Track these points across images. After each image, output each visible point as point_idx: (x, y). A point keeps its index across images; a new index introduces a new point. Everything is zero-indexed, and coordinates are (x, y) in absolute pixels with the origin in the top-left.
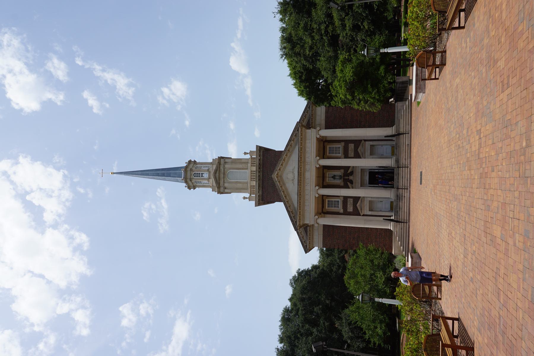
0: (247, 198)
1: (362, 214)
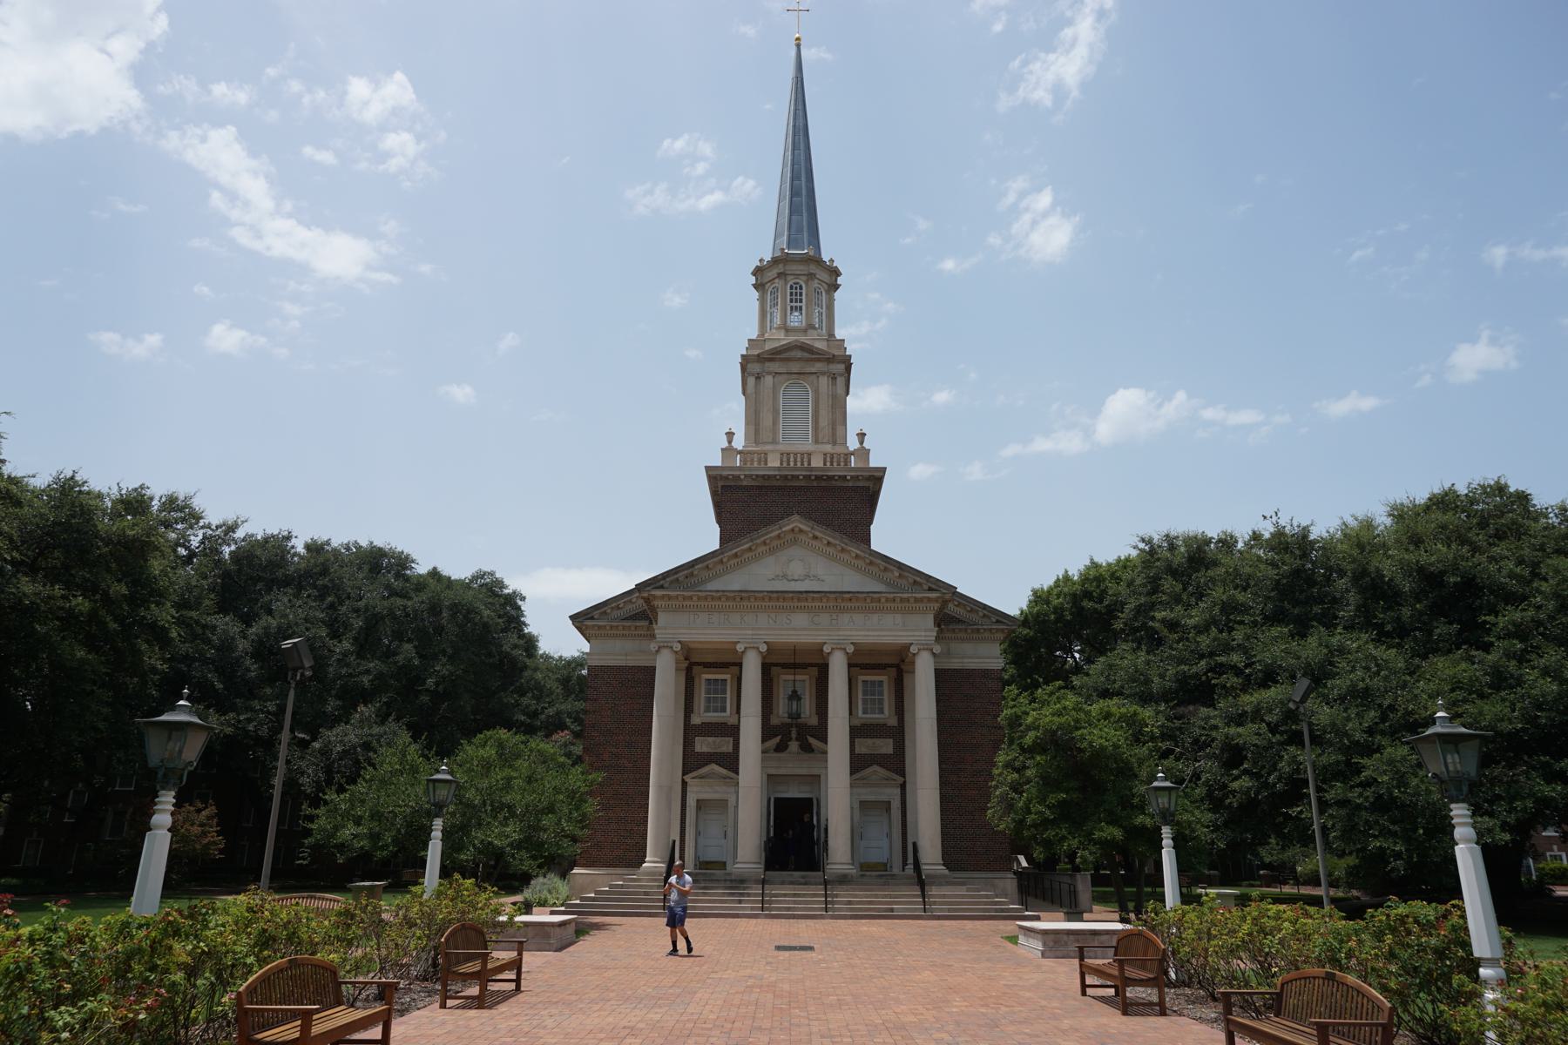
1: (687, 778)
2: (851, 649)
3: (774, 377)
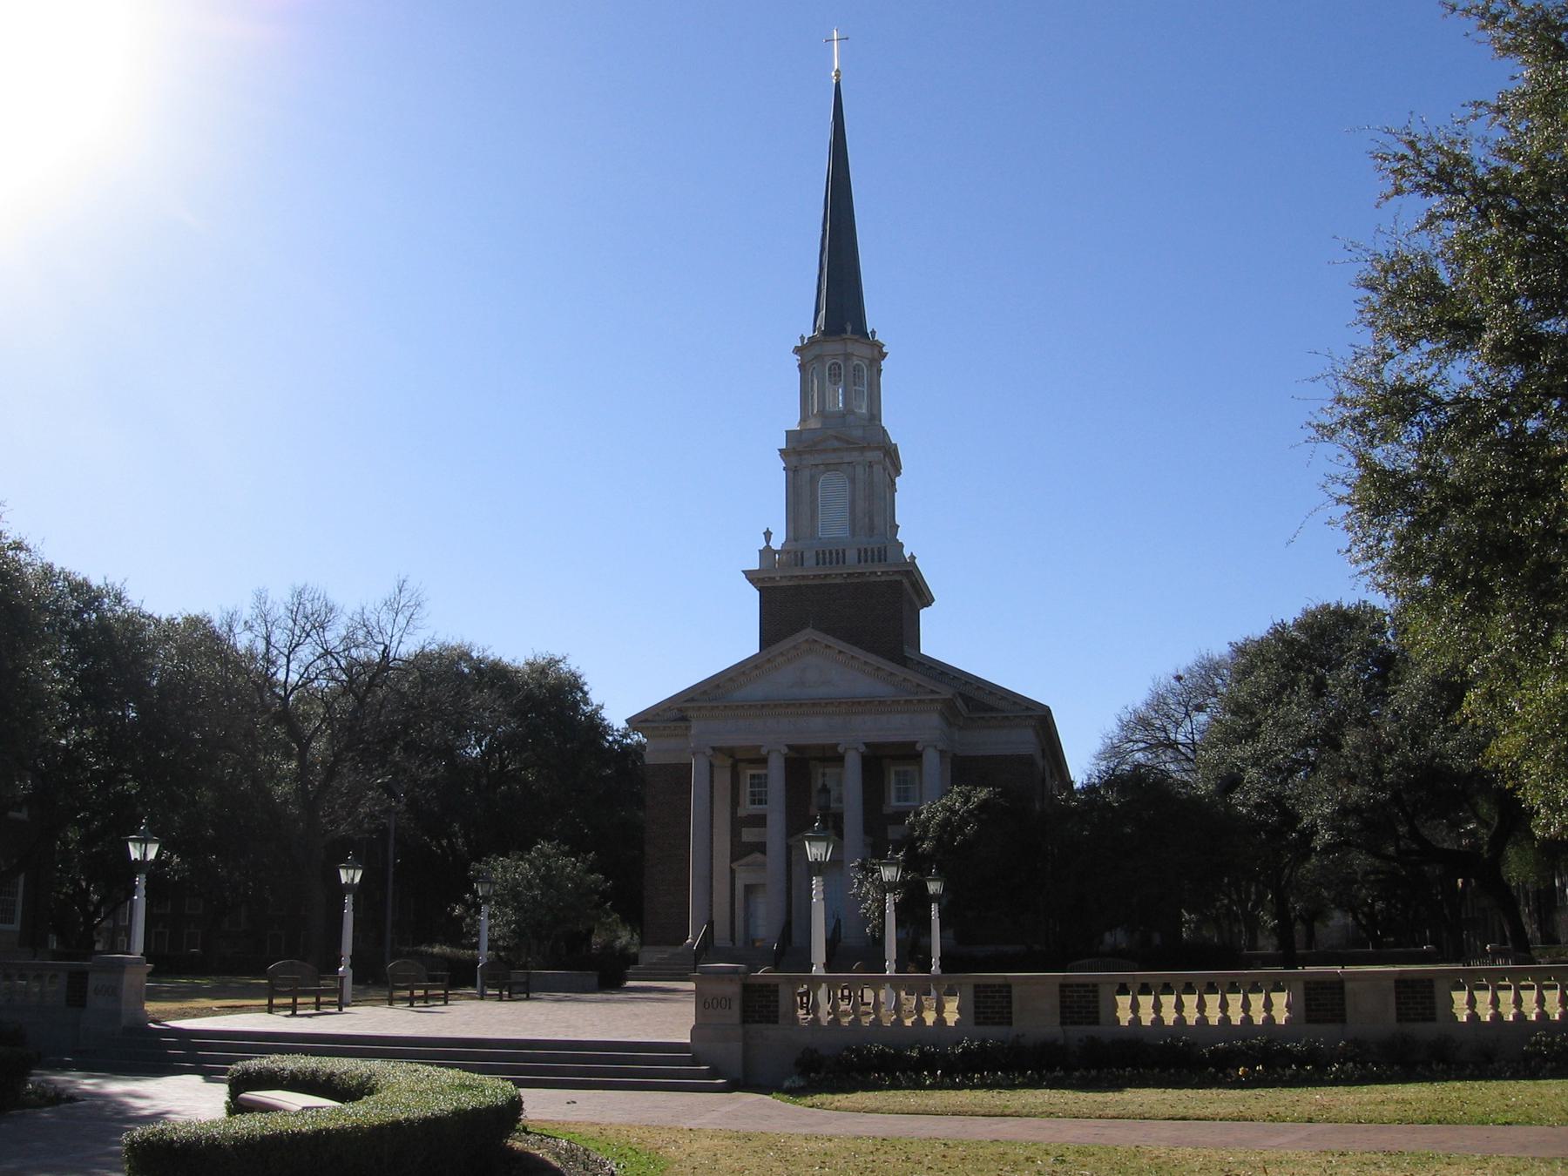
0: (768, 539)
1: (735, 866)
2: (863, 749)
3: (811, 470)
